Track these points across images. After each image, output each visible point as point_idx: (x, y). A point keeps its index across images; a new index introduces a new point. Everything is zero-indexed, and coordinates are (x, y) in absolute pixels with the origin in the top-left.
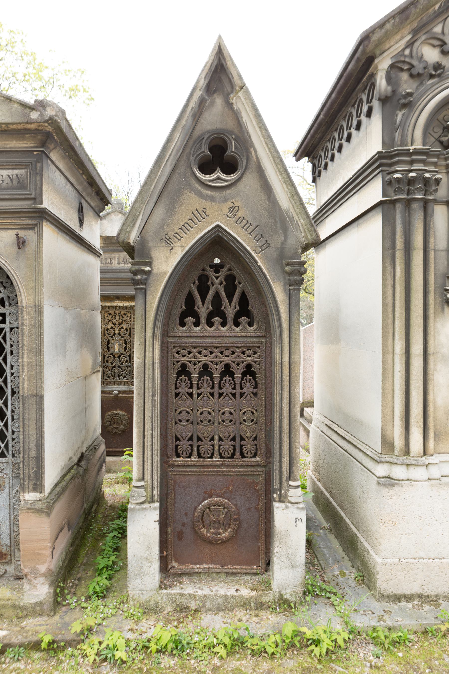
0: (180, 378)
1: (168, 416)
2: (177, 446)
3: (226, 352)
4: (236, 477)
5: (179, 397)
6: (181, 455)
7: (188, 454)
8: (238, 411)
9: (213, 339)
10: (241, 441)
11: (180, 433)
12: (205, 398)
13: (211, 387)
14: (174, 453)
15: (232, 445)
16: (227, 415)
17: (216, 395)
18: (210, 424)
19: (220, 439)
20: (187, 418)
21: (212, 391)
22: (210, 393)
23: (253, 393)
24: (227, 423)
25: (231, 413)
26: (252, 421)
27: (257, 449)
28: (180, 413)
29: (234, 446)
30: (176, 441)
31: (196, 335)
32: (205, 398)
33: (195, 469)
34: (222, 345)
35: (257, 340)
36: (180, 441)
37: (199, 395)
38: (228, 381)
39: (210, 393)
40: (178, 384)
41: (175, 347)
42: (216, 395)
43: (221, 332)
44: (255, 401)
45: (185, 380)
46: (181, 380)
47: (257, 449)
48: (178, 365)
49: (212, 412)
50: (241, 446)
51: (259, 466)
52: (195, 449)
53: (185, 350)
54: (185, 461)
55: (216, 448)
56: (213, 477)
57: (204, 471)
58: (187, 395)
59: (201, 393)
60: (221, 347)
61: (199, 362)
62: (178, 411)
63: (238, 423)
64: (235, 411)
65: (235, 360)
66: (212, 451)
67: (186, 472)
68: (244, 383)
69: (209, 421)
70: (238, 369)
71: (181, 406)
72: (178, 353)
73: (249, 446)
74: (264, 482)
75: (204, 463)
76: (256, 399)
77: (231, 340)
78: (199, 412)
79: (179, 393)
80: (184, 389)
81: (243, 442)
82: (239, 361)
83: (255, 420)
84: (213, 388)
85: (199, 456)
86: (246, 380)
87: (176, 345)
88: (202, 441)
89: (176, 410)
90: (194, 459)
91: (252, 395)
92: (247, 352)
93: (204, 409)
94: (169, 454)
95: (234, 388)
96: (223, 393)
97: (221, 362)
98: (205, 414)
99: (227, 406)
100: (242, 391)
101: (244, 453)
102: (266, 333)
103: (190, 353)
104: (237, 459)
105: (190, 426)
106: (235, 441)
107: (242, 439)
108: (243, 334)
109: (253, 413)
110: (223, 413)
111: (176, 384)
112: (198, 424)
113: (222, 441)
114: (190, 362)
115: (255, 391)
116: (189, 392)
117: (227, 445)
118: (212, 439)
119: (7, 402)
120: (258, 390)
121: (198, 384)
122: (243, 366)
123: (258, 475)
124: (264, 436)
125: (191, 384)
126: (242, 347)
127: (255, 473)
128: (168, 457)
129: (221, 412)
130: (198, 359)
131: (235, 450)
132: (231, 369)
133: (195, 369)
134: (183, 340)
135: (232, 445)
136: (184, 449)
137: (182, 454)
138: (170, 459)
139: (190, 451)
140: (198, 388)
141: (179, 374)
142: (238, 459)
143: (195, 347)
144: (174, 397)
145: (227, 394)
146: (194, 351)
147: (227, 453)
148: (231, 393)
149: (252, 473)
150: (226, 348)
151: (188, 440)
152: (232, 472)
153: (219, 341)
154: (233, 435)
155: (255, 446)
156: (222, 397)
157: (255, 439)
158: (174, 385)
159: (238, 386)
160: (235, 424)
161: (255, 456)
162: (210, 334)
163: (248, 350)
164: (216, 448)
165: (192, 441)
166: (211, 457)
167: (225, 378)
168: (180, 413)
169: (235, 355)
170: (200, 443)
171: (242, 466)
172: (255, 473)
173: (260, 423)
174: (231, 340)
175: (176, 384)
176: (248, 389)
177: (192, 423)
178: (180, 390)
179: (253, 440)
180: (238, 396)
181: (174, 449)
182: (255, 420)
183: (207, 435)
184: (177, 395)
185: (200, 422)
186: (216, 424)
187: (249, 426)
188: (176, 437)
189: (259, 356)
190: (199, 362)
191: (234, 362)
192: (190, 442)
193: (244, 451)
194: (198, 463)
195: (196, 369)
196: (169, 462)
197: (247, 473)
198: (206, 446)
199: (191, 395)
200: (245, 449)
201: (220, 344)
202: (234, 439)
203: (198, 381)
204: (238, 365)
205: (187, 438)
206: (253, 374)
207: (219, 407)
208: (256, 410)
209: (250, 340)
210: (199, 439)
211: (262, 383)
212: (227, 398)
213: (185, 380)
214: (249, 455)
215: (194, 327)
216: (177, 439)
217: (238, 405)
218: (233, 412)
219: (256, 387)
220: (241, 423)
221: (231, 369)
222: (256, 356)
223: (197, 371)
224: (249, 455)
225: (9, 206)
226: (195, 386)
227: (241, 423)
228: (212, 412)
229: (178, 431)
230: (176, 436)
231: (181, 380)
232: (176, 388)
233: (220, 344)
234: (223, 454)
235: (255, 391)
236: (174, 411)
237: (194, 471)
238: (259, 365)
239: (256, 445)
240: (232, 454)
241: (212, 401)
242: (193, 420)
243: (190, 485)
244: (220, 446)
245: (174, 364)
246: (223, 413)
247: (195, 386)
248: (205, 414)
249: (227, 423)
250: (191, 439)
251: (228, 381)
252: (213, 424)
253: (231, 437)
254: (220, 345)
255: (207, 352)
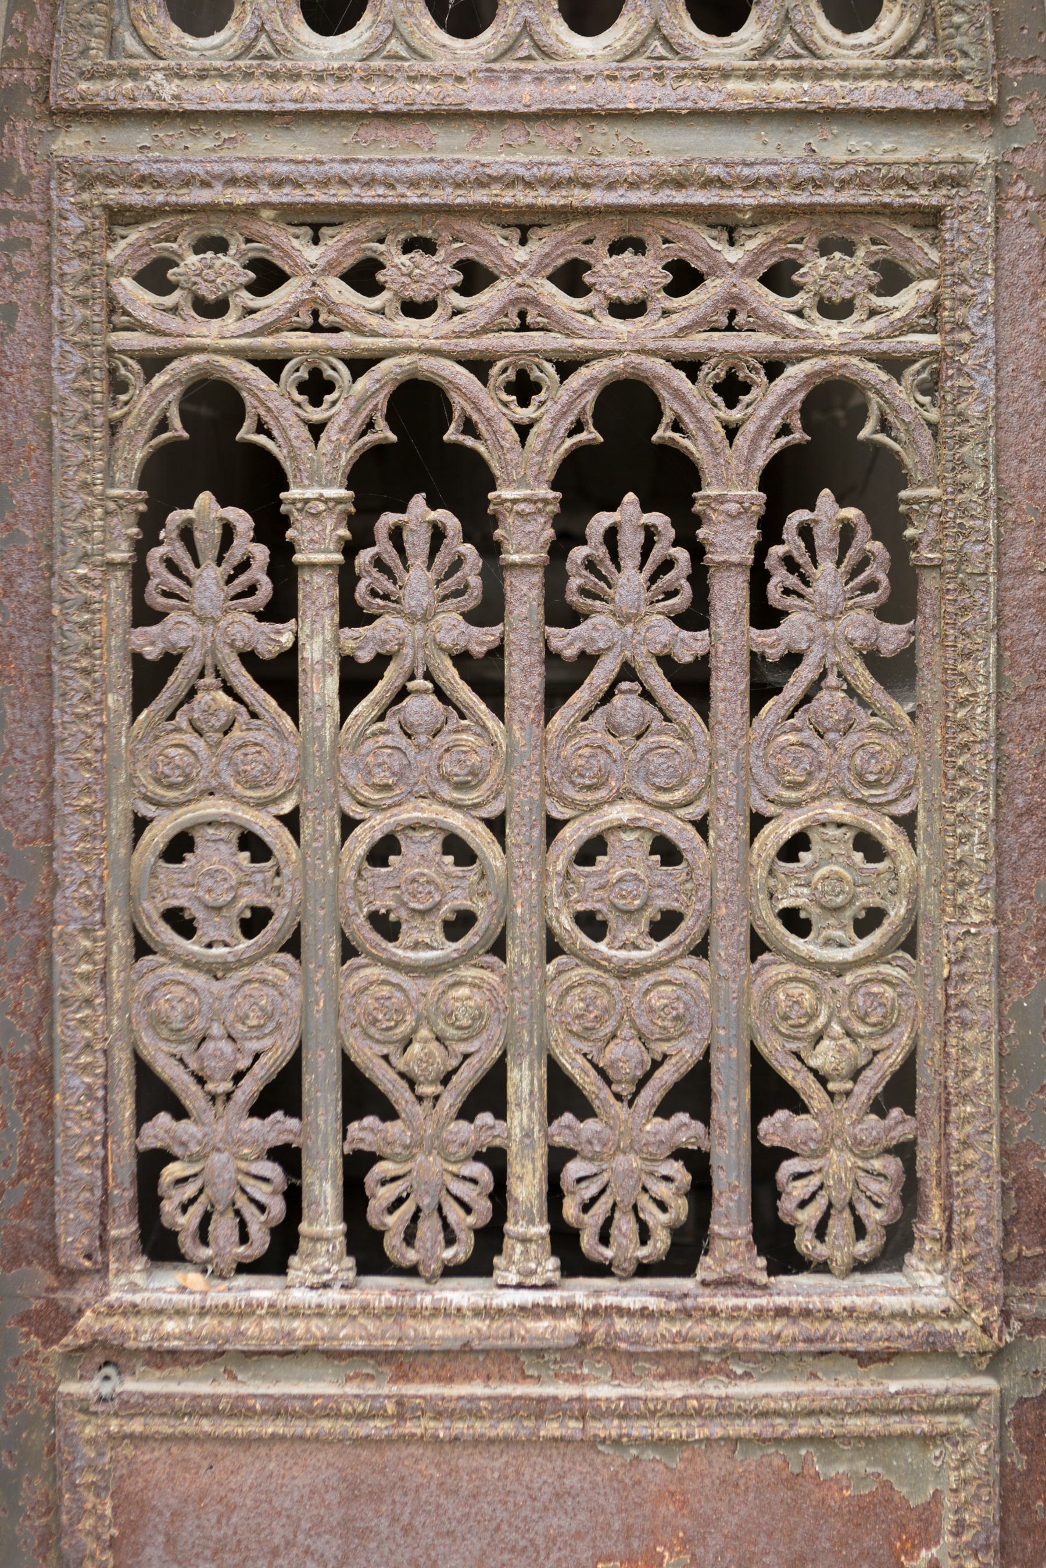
0: (177, 517)
1: (55, 885)
2: (150, 1163)
3: (618, 274)
4: (720, 1462)
5: (164, 700)
6: (187, 1243)
7: (260, 1242)
8: (727, 828)
9: (493, 138)
10: (760, 1109)
11: (177, 1035)
12: (421, 707)
13: (472, 600)
14: (125, 1229)
15: (679, 1154)
16: (628, 863)
17: (524, 679)
18: (466, 957)
19: (563, 1096)
20: (251, 897)
21: (480, 640)
22: (462, 660)
23: (872, 660)
24: (627, 946)
25: (667, 851)
26: (869, 921)
27: (911, 1191)
28: (179, 847)
29: (697, 1162)
30: (143, 1115)
31: (329, 96)
32: (421, 707)
33: (323, 1386)
34: (579, 197)
35: (908, 149)
36: (180, 1113)
37: (356, 680)
38: (630, 542)
39: (462, 660)
40: (160, 577)
41: (120, 217)
42: (524, 679)
43: (563, 76)
44: (894, 730)
45: (228, 532)
46: (186, 534)
47: (911, 1191)
48: (156, 398)
49: (480, 838)
50: (765, 1162)
51: (935, 1352)
52: (324, 1191)
53: (220, 246)
54: (225, 1311)
55: (527, 1186)
56: (494, 1464)
57: (404, 1409)
58: (244, 681)
59: (382, 661)
60: (564, 214)
61: (359, 365)
62: (162, 830)
63: (728, 946)
64: (702, 826)
65: (698, 342)
66: (484, 1208)
67: (240, 1409)
68: (790, 564)
69: (459, 924)
70: (731, 432)
71: (185, 785)
72: (156, 277)
73: (834, 1158)
74: (983, 1512)
75: (413, 1327)
76: (902, 710)
77: (665, 148)
78: (363, 839)
79: (170, 661)
80: (211, 619)
81: (776, 1128)
82: (730, 351)
83: (897, 911)
84: (489, 611)
85: (368, 1252)
86: (806, 532)
87: (135, 197)
88: (388, 1112)
89: (140, 824)
90: (319, 1283)
91: (865, 680)
92: (815, 269)
93: (408, 814)
94: (73, 1241)
95: (696, 617)
96: (587, 661)
97: (566, 368)
98: (421, 858)
99: (632, 773)
100: (772, 642)
101: (789, 1231)
102: (1002, 84)
103: (267, 277)
104: (728, 1282)
105: (278, 969)
106: (702, 1113)
107: (770, 1092)
108: (782, 86)
109: (869, 846)
110: (591, 851)
111: (139, 576)
112: (348, 951)
113: (584, 1110)
114: (272, 367)
115: (892, 637)
116: (267, 650)
117: (630, 1158)
118: (489, 1095)
119: (517, 210)
120: (927, 633)
121: (347, 578)
122: (771, 402)
123: (927, 1439)
124: (982, 1066)
125: (284, 569)
126: (766, 215)
127: (898, 1425)
128: (70, 1276)
129: (572, 837)
130: (344, 340)
131: (701, 1192)
132: (663, 433)
133: (316, 430)
134: (198, 152)
135: (679, 1154)
136: (222, 1191)
137: (203, 1235)
138: (83, 1293)
139: (277, 1207)
140: (352, 615)
141: (169, 480)
142: (733, 1293)
143: (316, 222)
144: (118, 700)
145: (627, 672)
146: (312, 254)
147: (625, 1226)
148: (666, 662)
149: (873, 1424)
150: (611, 232)
151: (260, 1108)
152: (679, 1412)
153: (547, 153)
154: (683, 1055)
155: (892, 1165)
156: (581, 697)
157: (900, 1091)
158: (120, 583)
159: (730, 594)
160: (701, 950)
161: (893, 1251)
162: (453, 95)
163: (825, 248)
164: (527, 1186)
165: (294, 1110)
166: (479, 1265)
167: (601, 521)
168: (179, 847)
169: (698, 299)
170: (367, 1131)
171: (773, 1360)
172: (898, 1425)
173: (939, 945)
174: (665, 148)
175: (139, 576)
176: (829, 619)
177: (293, 946)
178: (178, 630)
179: (879, 1107)
180: (729, 685)
181: (124, 1194)
182: (897, 911)
183: (441, 1060)
184: (149, 678)
185: (367, 936)
186: (524, 951)
187: (840, 969)
188: (144, 1074)
189: (936, 306)
190: (359, 365)
191: (691, 367)
192: (279, 1128)
193: (786, 1206)
194: (351, 1335)
195: (331, 433)
196: (64, 1319)
197: (827, 1425)
198: (425, 1157)
199: (280, 677)
200: (799, 1190)
201: (555, 184)
202: (692, 1094)
203: (350, 550)
204: (732, 389)
205: (250, 1088)
206: (873, 481)
207: (547, 789)
208: (907, 823)
209: (845, 147)
210: (361, 1096)
211: (962, 559)
212: (627, 704)
213: (228, 532)
214: (840, 1245)
215: (306, 33)
216: (154, 1096)
217: (727, 768)
218: (685, 837)
219: (899, 607)
220: (757, 947)
221: (663, 433)
222: (906, 301)
223: (340, 448)
224: (840, 1245)
225: (861, 182)
226: (318, 593)
227: (757, 947)
228: (480, 838)
229: (158, 1022)
230: (143, 1070)
231: (186, 534)
232: (145, 615)
233: (555, 184)
234: (588, 1242)
235: (892, 637)
236: (120, 828)
237: (312, 1409)
238: (930, 387)
239: (905, 1151)
240: (676, 1232)
241: (481, 736)
242: (299, 910)
243: (279, 1534)
244: (558, 1157)
245: (118, 386)
246: (591, 851)
247: (318, 593)
248: (421, 858)
249: (627, 946)
250: (282, 1094)
251: (630, 542)
252: (499, 948)
253: (667, 1076)
254: (555, 199)
255: (434, 273)
